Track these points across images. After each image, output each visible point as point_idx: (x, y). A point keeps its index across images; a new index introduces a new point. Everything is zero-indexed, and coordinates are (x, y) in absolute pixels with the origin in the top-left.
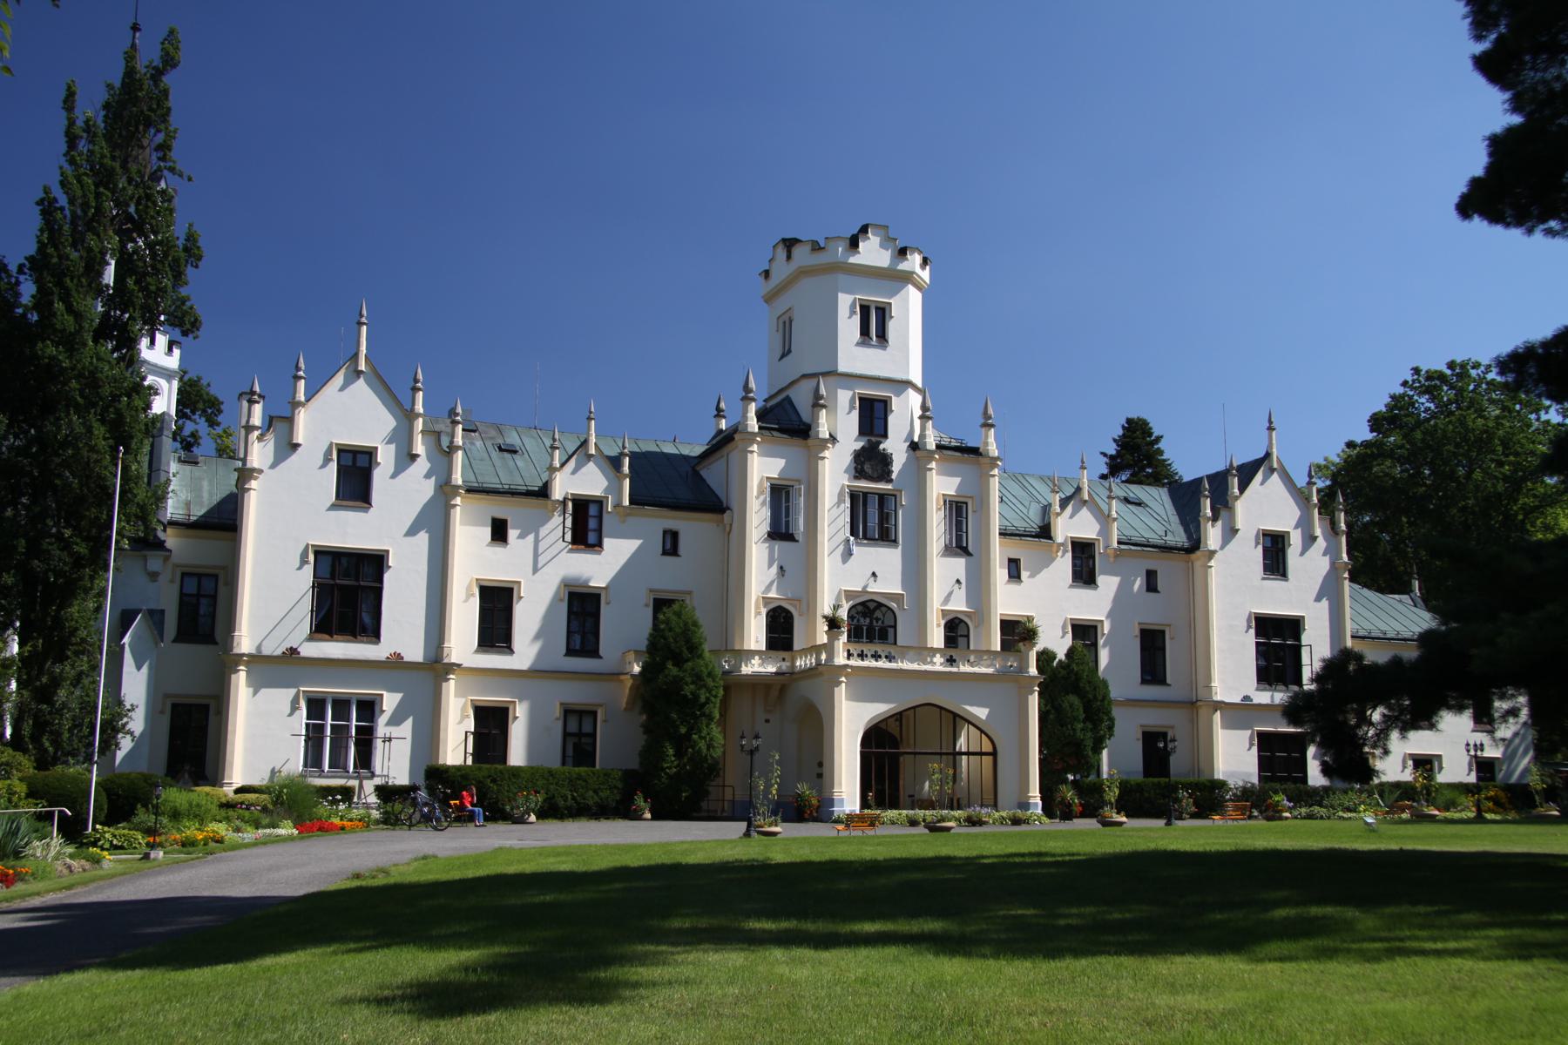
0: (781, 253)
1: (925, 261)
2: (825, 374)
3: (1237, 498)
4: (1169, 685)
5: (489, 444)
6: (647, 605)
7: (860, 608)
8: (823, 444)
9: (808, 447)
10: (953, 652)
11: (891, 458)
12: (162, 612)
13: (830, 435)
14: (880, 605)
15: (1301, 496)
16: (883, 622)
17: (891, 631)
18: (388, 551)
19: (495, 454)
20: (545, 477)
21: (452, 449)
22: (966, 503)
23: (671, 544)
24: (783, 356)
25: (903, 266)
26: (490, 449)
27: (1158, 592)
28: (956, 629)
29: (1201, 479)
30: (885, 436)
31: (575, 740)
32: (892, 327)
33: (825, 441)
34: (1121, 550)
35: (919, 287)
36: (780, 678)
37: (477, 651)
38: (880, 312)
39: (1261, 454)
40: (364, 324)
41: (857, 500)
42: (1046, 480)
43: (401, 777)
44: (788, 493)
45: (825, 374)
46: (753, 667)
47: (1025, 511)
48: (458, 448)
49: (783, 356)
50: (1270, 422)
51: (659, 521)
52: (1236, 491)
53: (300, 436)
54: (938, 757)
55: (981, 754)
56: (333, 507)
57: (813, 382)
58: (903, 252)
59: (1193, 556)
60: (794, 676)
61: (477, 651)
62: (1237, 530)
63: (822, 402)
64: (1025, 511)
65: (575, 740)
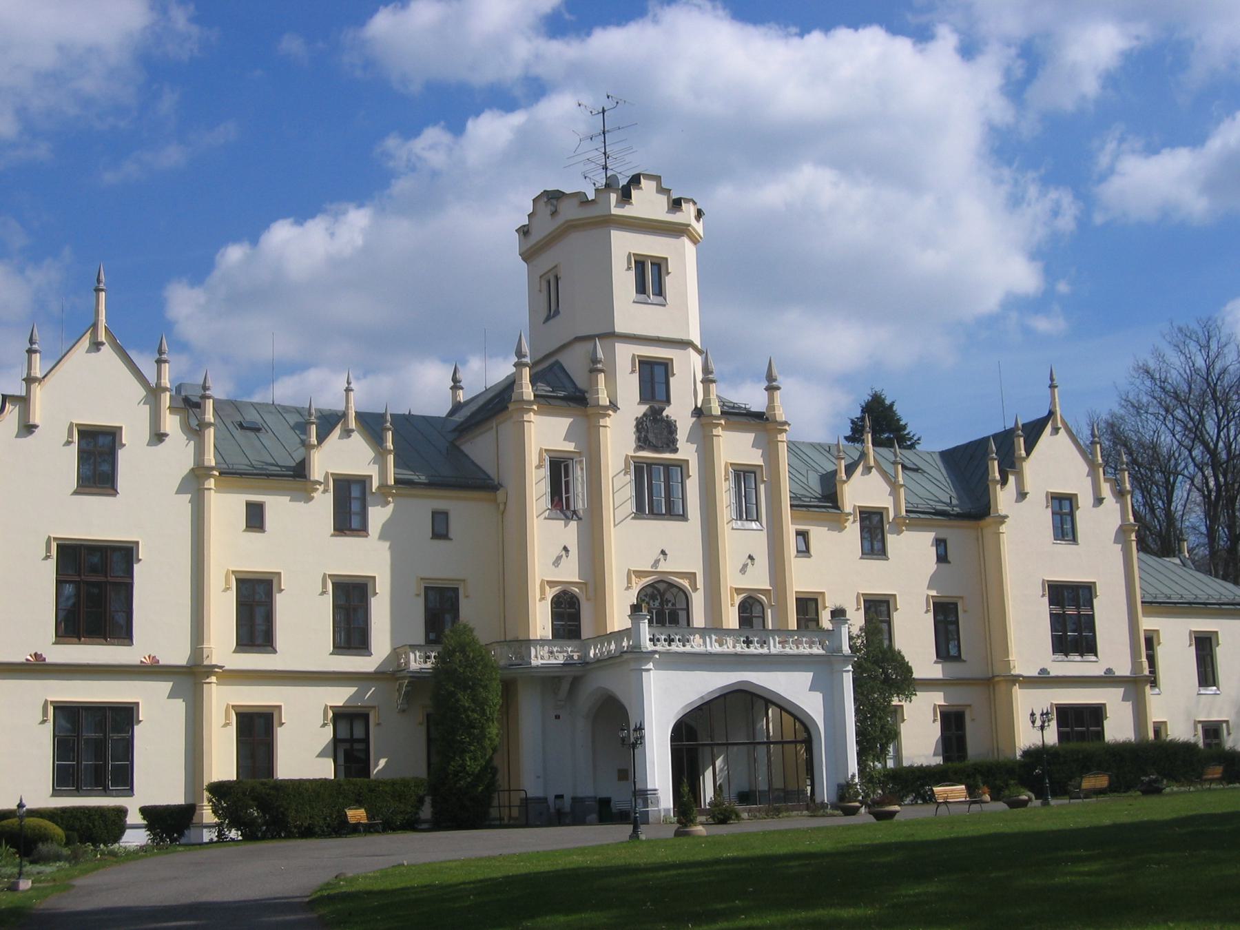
0: (545, 211)
1: (699, 214)
2: (602, 336)
3: (1024, 459)
4: (964, 661)
5: (228, 422)
6: (418, 595)
7: (649, 591)
8: (603, 412)
9: (587, 416)
10: (748, 632)
11: (675, 426)
12: (695, 574)
13: (610, 402)
14: (671, 585)
15: (1086, 453)
16: (673, 605)
17: (682, 614)
18: (137, 543)
19: (238, 433)
20: (298, 457)
21: (203, 425)
22: (755, 473)
23: (440, 528)
24: (548, 318)
25: (677, 218)
26: (231, 427)
27: (949, 562)
28: (750, 608)
29: (984, 442)
30: (668, 401)
31: (347, 746)
32: (669, 282)
33: (606, 408)
34: (910, 519)
35: (695, 241)
36: (568, 669)
37: (236, 651)
38: (656, 267)
39: (1046, 413)
40: (102, 290)
41: (641, 470)
42: (818, 447)
43: (174, 796)
44: (566, 467)
45: (602, 336)
46: (539, 658)
47: (804, 480)
48: (210, 425)
49: (548, 318)
50: (1052, 379)
51: (423, 507)
52: (1023, 453)
53: (37, 417)
54: (725, 747)
55: (795, 742)
56: (76, 493)
57: (588, 346)
58: (676, 204)
59: (983, 523)
60: (589, 667)
61: (236, 651)
62: (1026, 494)
63: (599, 366)
64: (804, 480)
65: (347, 746)
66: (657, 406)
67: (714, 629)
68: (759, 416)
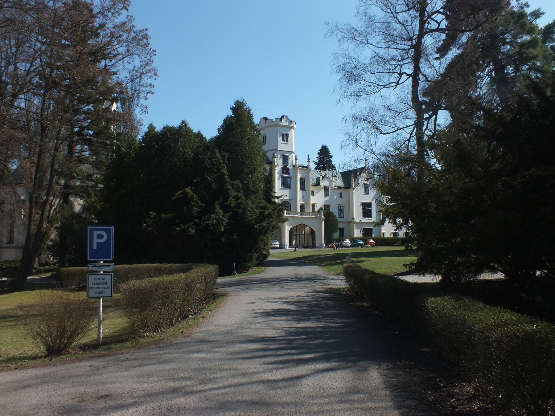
30: (288, 164)
32: (289, 138)
66: (286, 165)
67: (296, 212)
68: (305, 167)
